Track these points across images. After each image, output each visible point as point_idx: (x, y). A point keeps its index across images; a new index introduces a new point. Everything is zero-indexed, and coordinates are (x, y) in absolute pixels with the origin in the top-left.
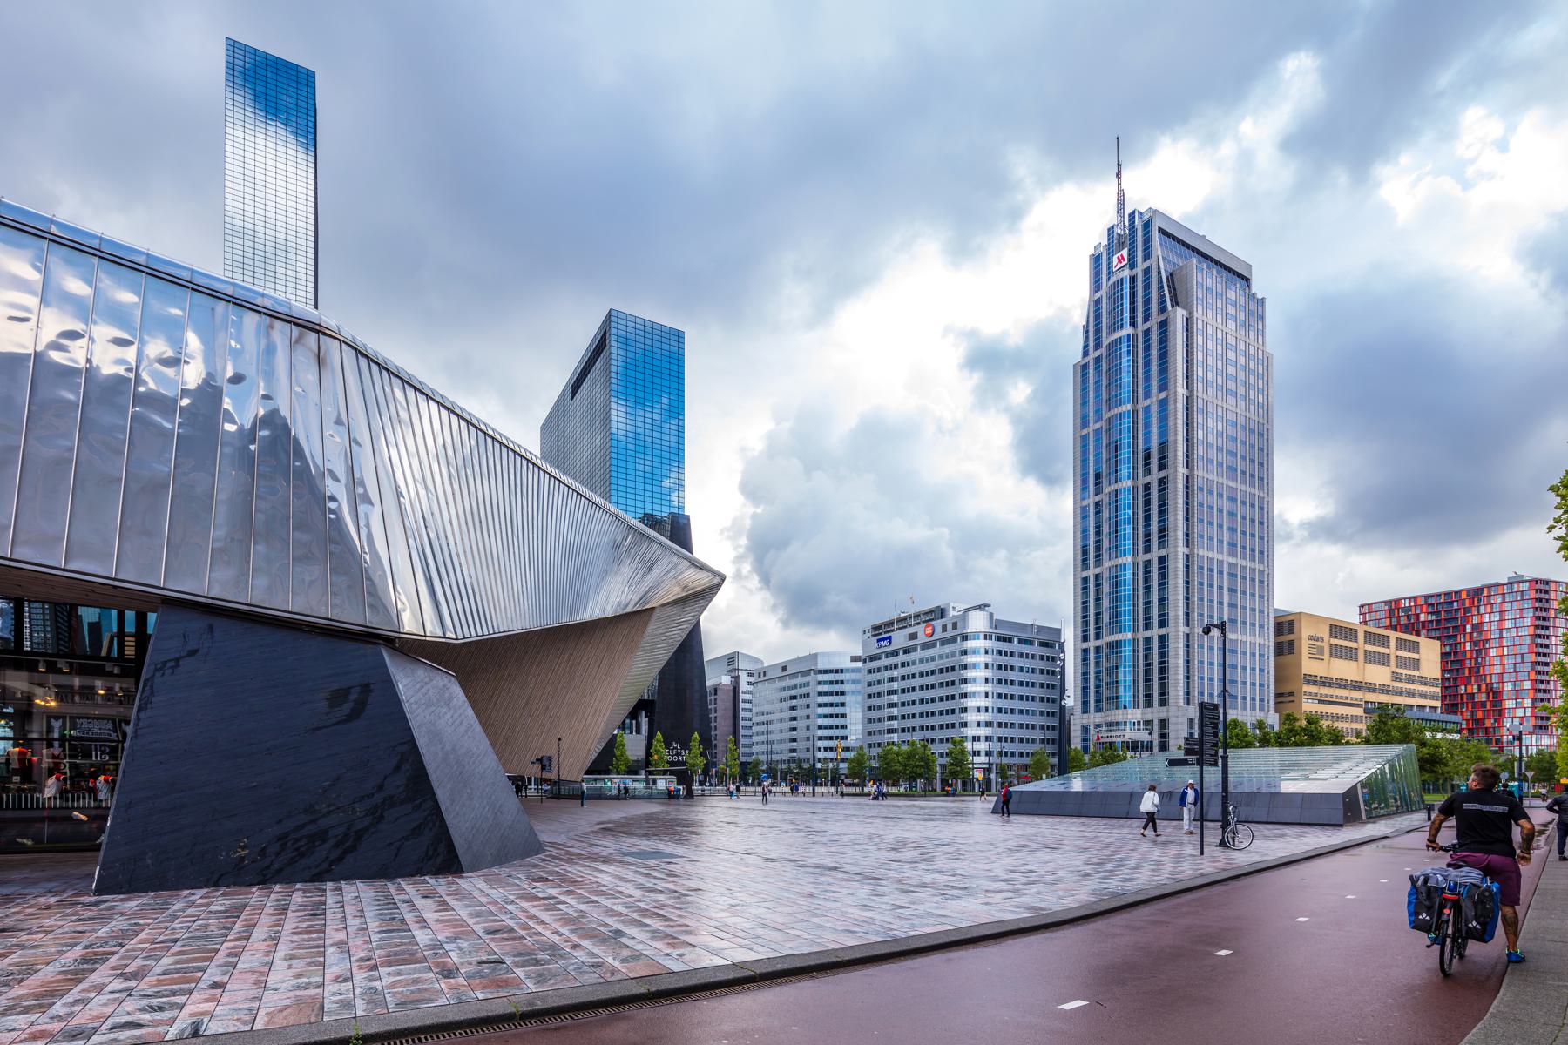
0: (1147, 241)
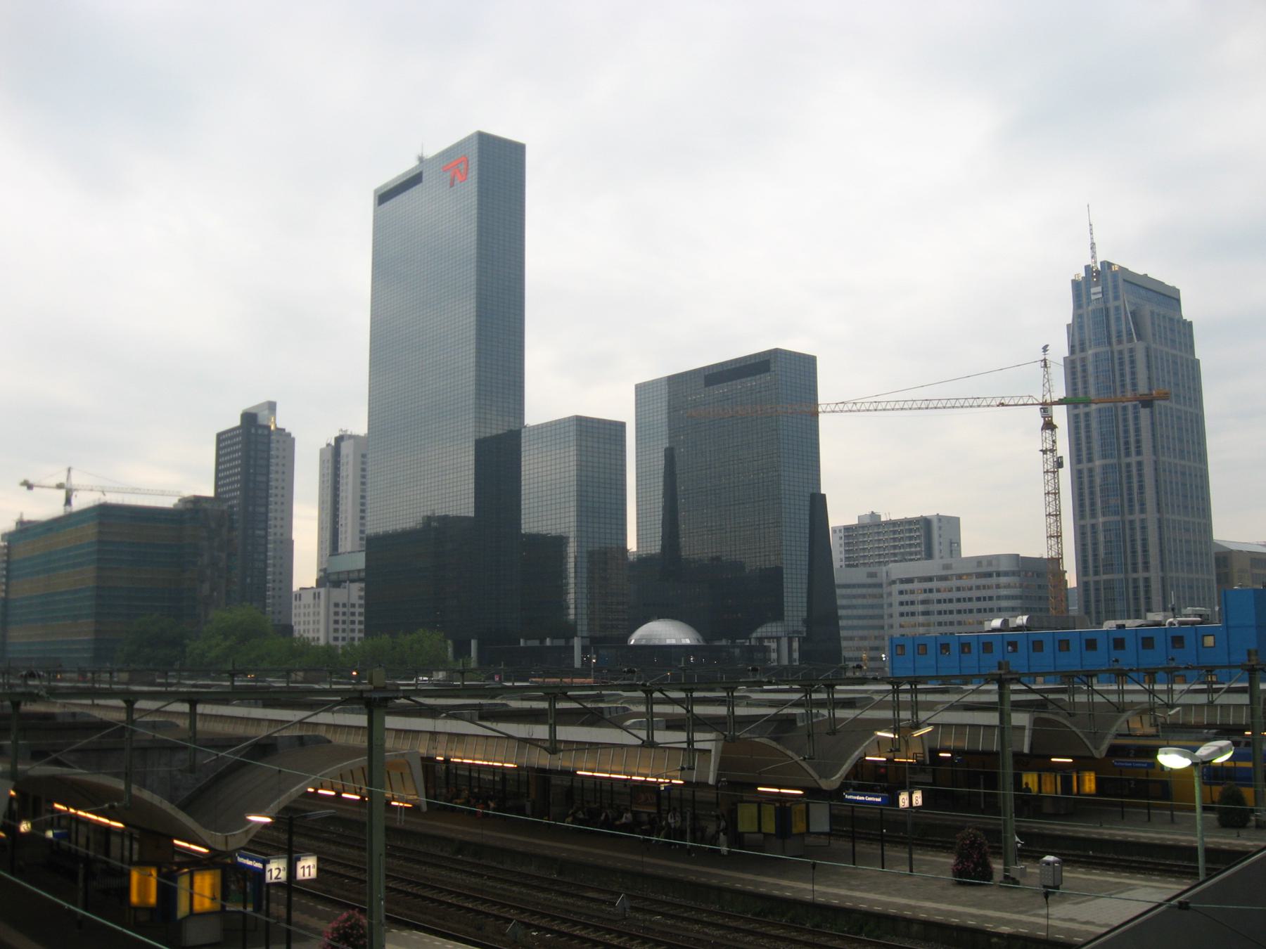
0: (1116, 287)
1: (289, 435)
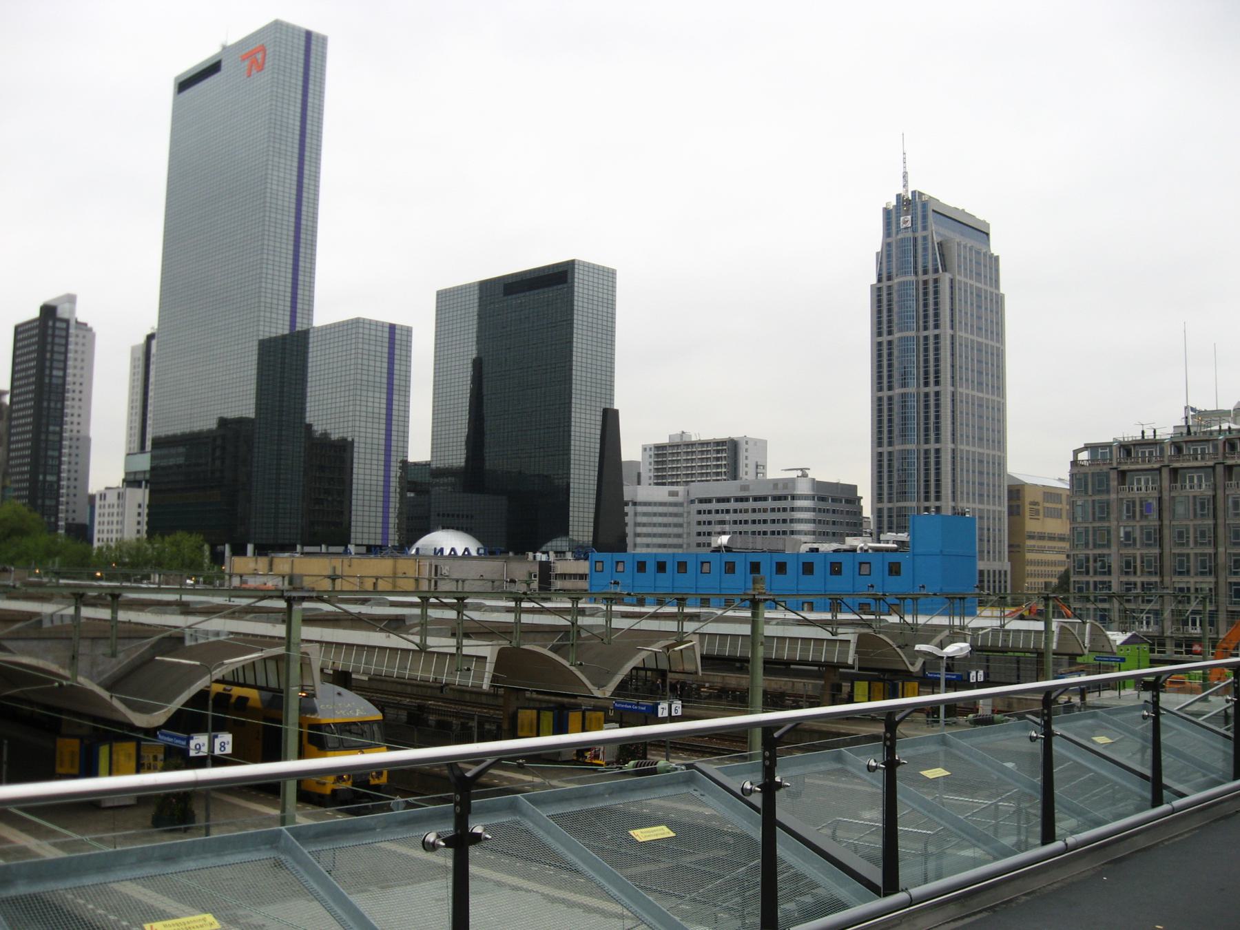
0: (925, 217)
1: (90, 330)
